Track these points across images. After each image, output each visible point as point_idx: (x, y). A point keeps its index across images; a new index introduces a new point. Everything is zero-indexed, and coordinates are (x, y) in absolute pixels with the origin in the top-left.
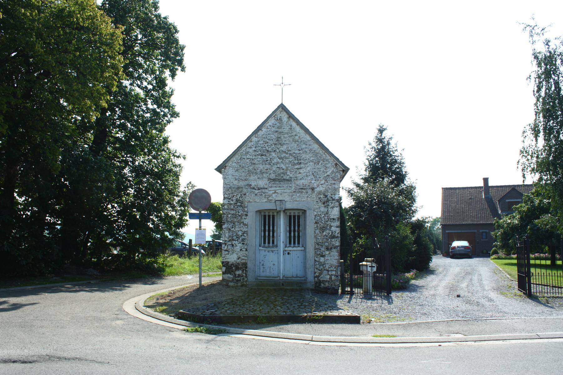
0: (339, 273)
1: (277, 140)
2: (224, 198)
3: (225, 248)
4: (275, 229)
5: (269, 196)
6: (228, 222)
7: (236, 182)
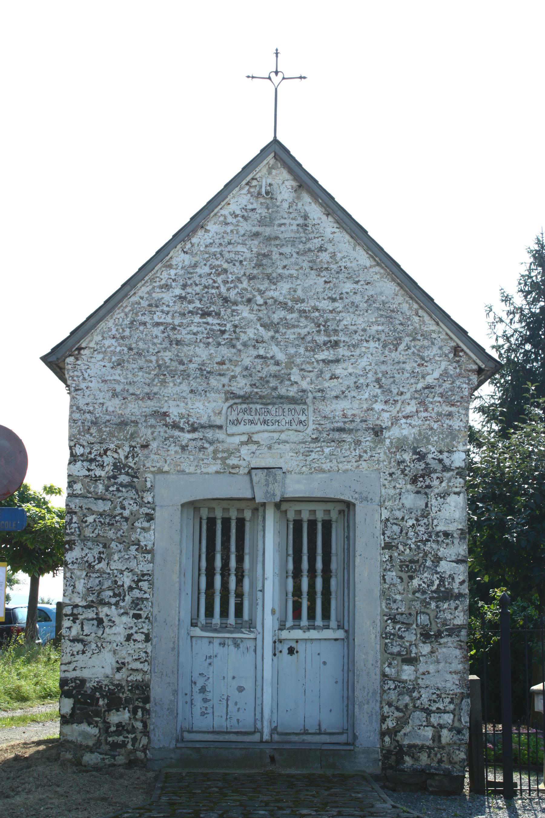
0: (465, 719)
1: (259, 265)
2: (74, 459)
3: (74, 632)
4: (247, 565)
5: (230, 453)
6: (85, 540)
7: (113, 405)
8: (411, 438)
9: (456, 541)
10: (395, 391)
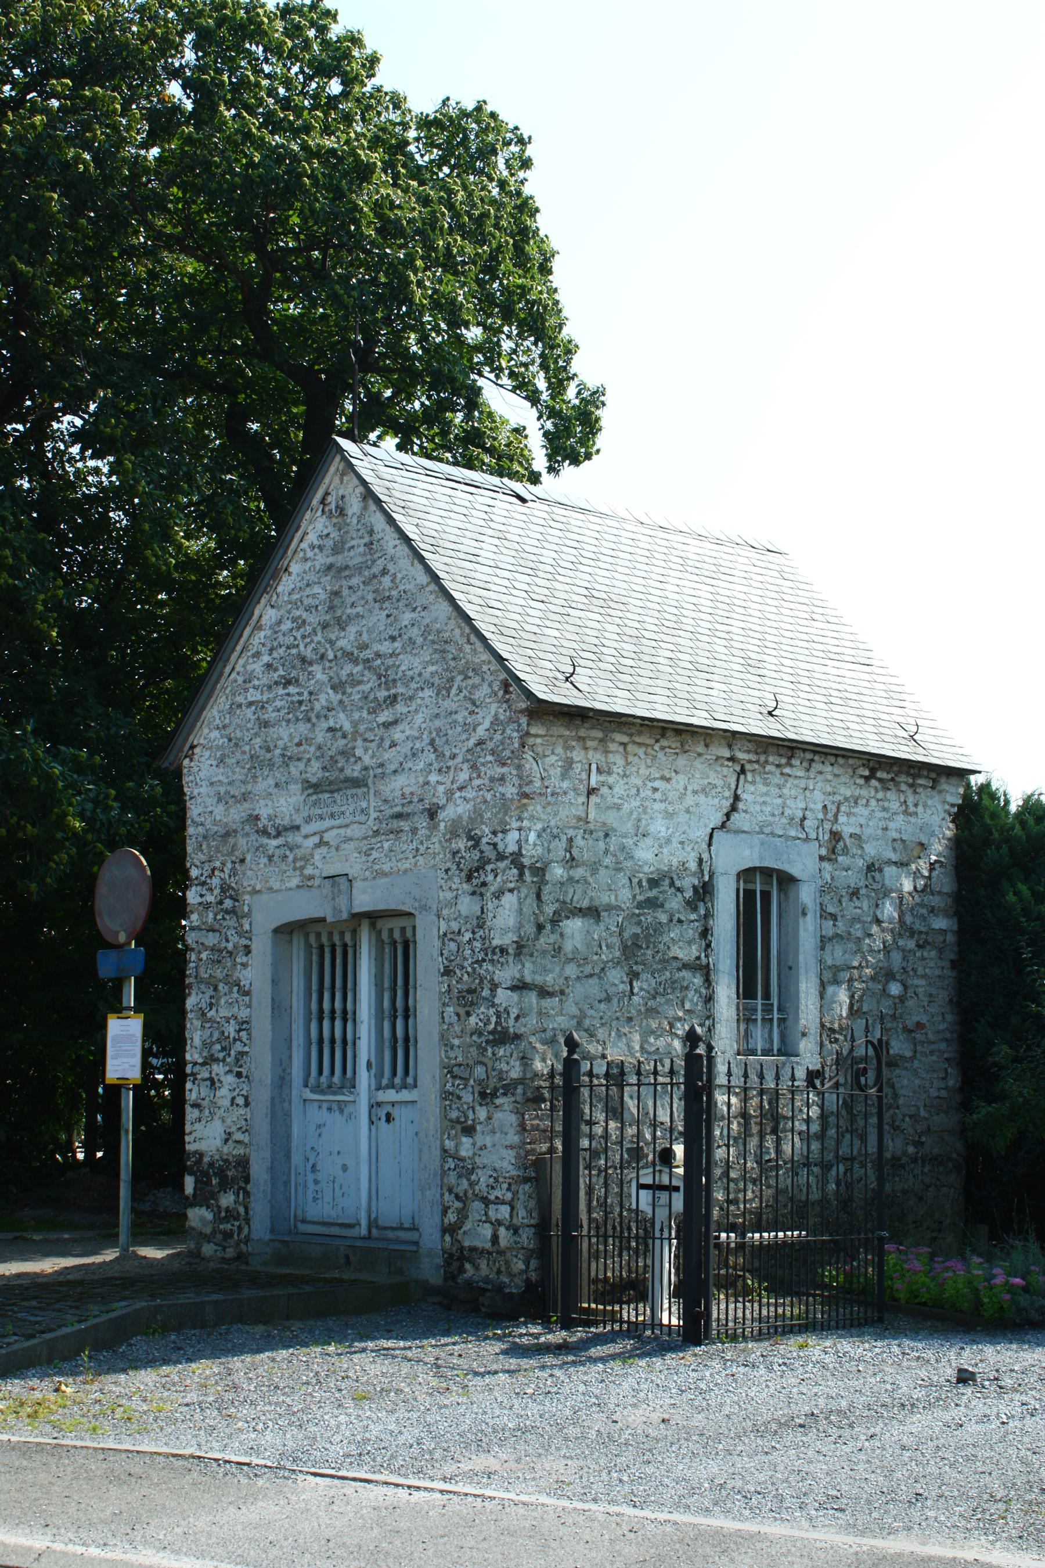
1: (332, 608)
8: (465, 818)
9: (511, 959)
10: (448, 754)
